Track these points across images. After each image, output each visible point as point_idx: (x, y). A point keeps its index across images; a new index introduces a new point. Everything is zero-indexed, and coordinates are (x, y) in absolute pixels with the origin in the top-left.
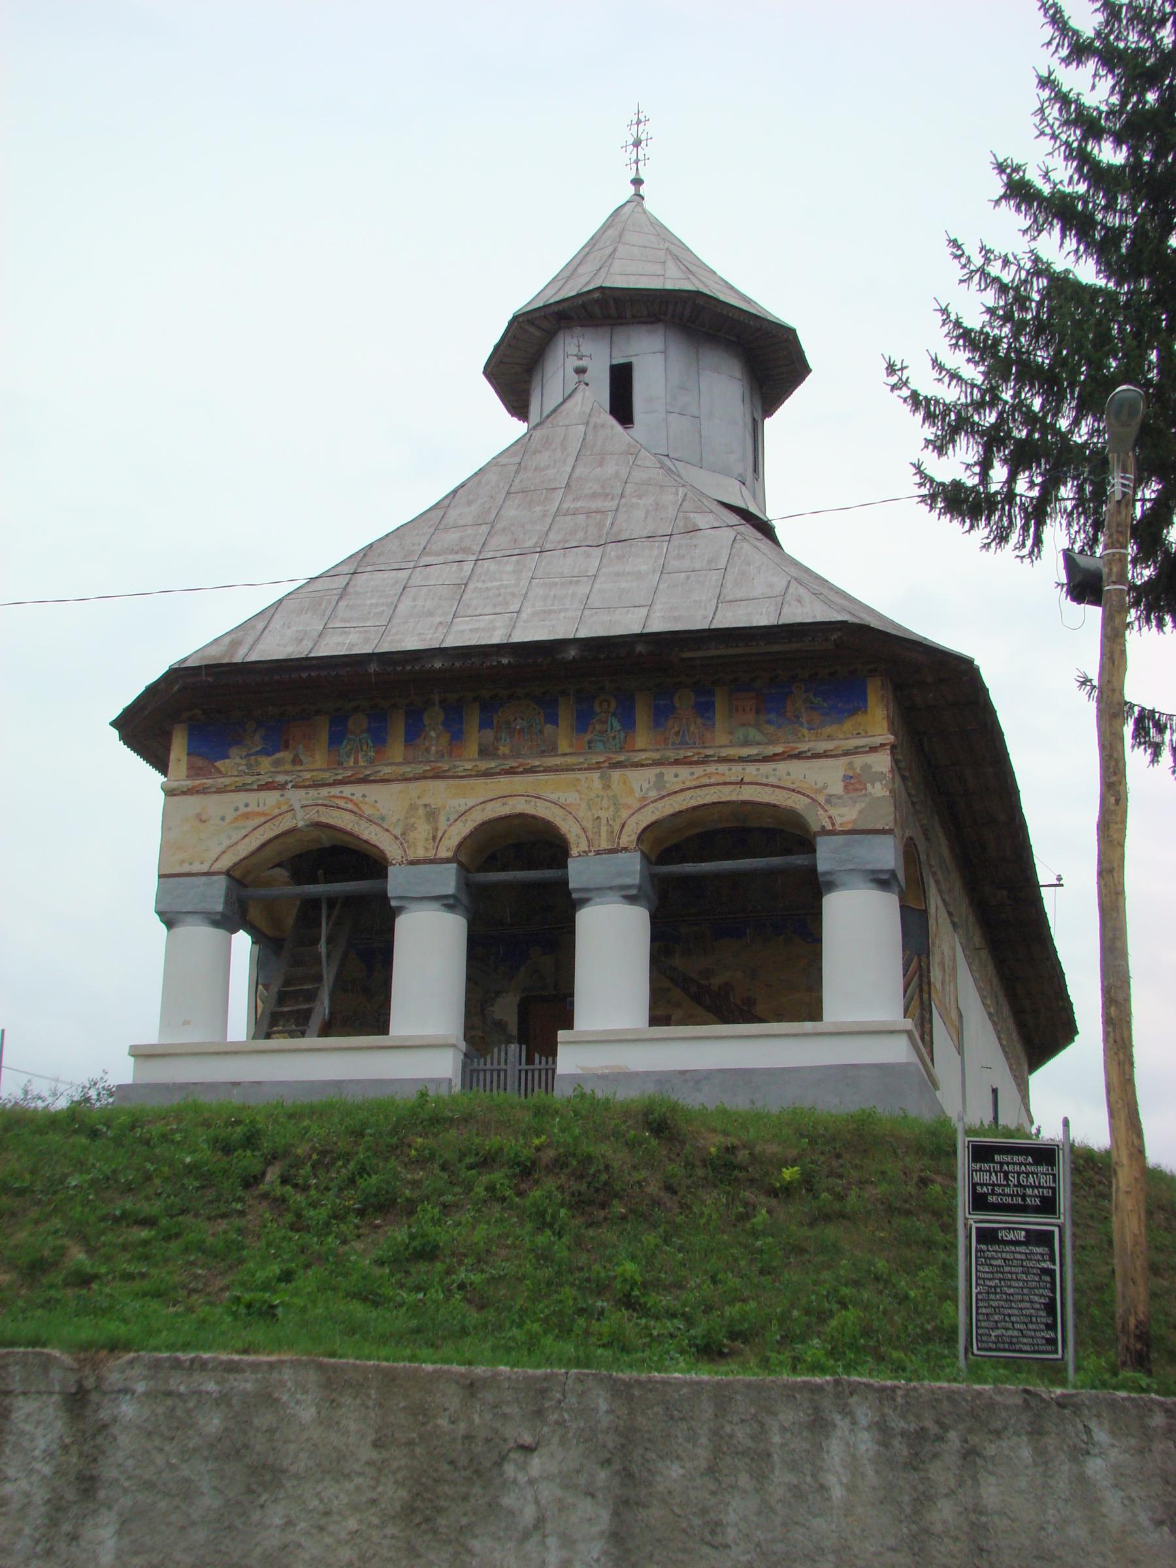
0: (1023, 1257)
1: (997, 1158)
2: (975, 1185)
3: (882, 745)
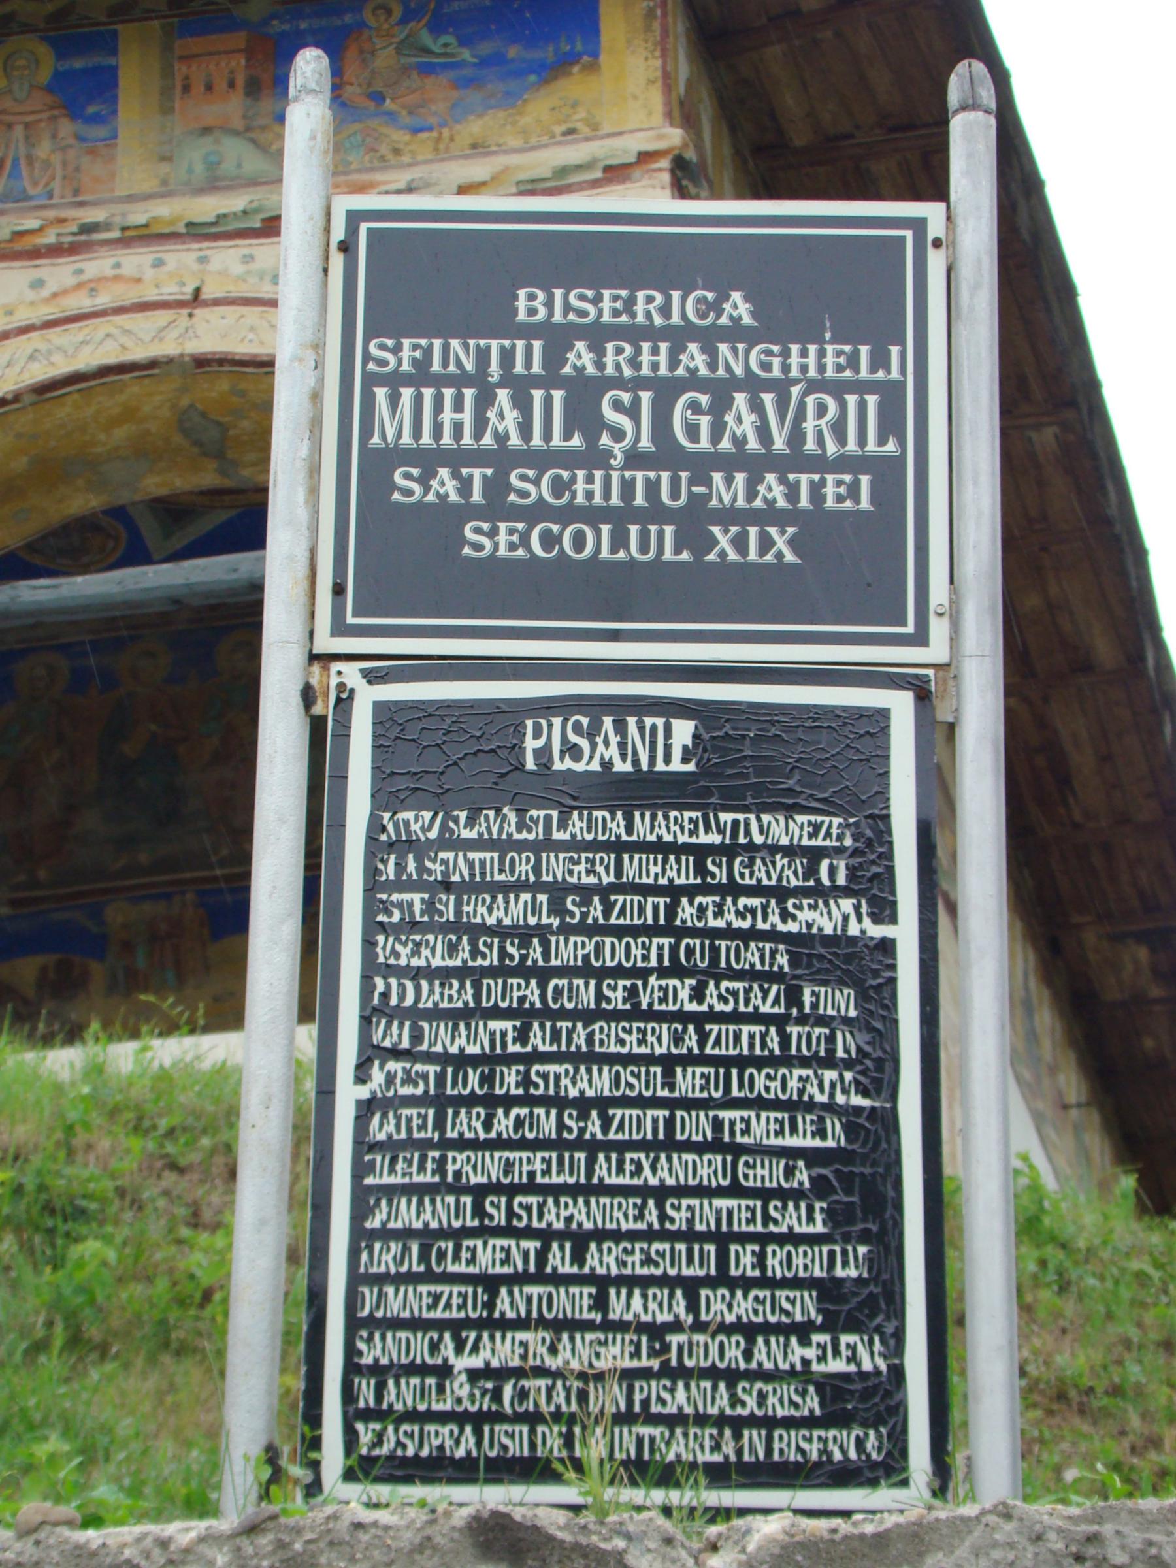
0: (681, 874)
1: (529, 304)
2: (379, 464)
3: (645, 157)
